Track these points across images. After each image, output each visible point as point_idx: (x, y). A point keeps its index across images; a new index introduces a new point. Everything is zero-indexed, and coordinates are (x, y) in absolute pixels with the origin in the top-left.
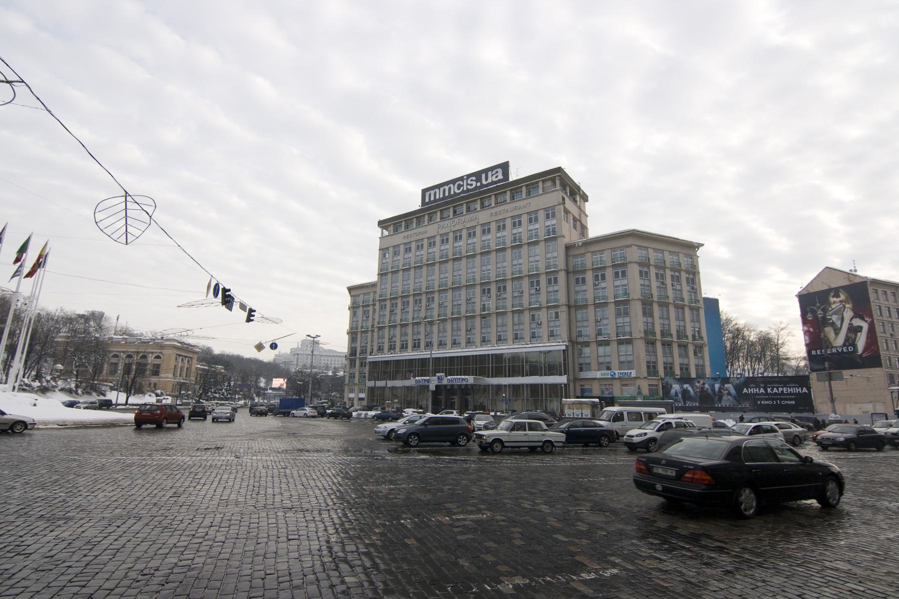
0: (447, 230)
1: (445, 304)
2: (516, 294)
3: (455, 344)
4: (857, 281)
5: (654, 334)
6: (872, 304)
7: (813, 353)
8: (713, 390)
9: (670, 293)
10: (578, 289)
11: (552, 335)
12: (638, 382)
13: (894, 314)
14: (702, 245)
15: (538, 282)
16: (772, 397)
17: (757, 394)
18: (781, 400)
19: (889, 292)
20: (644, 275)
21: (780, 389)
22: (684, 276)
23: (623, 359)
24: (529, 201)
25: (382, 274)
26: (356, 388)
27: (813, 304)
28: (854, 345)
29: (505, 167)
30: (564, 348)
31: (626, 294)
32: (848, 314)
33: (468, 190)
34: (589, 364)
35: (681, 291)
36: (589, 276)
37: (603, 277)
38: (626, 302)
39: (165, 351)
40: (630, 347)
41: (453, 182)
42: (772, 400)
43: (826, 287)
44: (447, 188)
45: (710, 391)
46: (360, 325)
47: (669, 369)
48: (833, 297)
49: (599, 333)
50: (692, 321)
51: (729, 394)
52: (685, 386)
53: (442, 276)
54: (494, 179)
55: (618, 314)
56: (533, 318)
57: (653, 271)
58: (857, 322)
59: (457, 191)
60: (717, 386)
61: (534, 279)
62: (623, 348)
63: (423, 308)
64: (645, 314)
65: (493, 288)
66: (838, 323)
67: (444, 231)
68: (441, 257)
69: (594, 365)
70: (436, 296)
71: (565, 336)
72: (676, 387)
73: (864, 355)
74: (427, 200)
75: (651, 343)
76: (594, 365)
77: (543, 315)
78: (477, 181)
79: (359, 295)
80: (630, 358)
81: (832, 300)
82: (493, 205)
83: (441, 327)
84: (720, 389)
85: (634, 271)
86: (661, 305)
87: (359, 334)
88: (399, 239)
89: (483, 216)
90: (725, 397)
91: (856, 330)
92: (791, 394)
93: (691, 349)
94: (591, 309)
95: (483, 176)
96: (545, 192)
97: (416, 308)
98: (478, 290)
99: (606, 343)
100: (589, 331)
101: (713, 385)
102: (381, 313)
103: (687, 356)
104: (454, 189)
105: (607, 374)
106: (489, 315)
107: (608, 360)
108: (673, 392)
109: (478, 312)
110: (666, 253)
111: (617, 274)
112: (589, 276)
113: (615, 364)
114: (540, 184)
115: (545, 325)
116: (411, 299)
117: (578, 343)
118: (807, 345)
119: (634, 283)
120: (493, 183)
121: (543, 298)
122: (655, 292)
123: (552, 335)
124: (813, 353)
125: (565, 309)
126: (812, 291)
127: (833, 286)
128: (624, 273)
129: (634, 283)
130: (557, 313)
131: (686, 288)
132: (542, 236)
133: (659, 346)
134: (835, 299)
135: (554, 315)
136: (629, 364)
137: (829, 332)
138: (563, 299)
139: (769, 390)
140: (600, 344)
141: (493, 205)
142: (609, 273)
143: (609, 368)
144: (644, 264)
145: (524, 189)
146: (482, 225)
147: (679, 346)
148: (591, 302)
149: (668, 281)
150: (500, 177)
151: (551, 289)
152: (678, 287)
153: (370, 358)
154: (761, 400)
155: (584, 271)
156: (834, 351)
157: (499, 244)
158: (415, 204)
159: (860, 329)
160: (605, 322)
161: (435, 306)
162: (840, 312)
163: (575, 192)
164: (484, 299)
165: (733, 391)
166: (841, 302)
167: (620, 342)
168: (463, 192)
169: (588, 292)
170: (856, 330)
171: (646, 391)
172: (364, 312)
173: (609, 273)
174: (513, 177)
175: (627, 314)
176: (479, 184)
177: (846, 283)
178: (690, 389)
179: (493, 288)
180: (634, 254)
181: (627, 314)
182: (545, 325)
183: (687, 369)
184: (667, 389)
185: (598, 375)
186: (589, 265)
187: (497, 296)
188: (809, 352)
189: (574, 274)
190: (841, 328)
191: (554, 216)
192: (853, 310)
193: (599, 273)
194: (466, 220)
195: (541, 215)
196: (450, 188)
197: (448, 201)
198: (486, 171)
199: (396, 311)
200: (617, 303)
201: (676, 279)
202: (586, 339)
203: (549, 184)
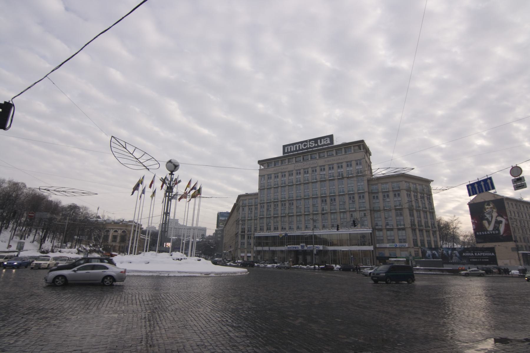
0: (300, 168)
1: (300, 207)
2: (341, 203)
4: (499, 198)
5: (415, 225)
6: (507, 210)
7: (478, 233)
8: (448, 254)
9: (421, 205)
10: (374, 201)
12: (410, 250)
13: (528, 217)
14: (432, 181)
17: (470, 256)
18: (482, 259)
19: (514, 204)
20: (409, 195)
21: (481, 254)
23: (400, 238)
24: (346, 156)
25: (261, 188)
26: (246, 251)
28: (498, 230)
29: (331, 137)
30: (371, 232)
32: (495, 214)
33: (310, 148)
34: (383, 240)
35: (425, 203)
36: (380, 195)
37: (388, 196)
38: (401, 209)
40: (404, 232)
41: (301, 142)
42: (478, 259)
43: (482, 200)
44: (298, 145)
45: (446, 254)
46: (247, 216)
47: (422, 242)
48: (487, 205)
49: (387, 224)
50: (431, 219)
51: (456, 256)
52: (434, 252)
53: (298, 192)
54: (325, 143)
55: (397, 215)
57: (412, 194)
58: (500, 219)
59: (304, 148)
60: (450, 252)
61: (351, 196)
62: (400, 232)
63: (287, 209)
64: (410, 215)
65: (328, 200)
66: (490, 219)
67: (298, 168)
68: (297, 182)
70: (295, 202)
71: (370, 225)
72: (429, 252)
73: (504, 235)
74: (286, 151)
75: (414, 230)
78: (315, 143)
79: (246, 200)
80: (404, 237)
81: (486, 207)
82: (326, 156)
83: (298, 219)
84: (451, 253)
85: (404, 193)
86: (417, 211)
87: (246, 221)
88: (272, 170)
89: (321, 162)
90: (454, 258)
91: (498, 223)
92: (486, 256)
93: (431, 232)
95: (319, 141)
96: (355, 152)
97: (282, 208)
98: (319, 200)
99: (392, 230)
100: (381, 223)
101: (448, 252)
102: (261, 210)
106: (327, 213)
107: (393, 238)
108: (427, 254)
110: (411, 184)
111: (395, 195)
112: (380, 195)
113: (397, 240)
114: (352, 147)
116: (279, 204)
117: (376, 229)
118: (474, 229)
119: (404, 198)
120: (324, 145)
121: (357, 206)
122: (414, 204)
124: (478, 233)
125: (369, 212)
126: (475, 202)
127: (487, 200)
128: (399, 195)
129: (404, 198)
130: (365, 214)
131: (427, 202)
133: (417, 231)
134: (488, 207)
135: (363, 215)
136: (405, 241)
137: (485, 223)
138: (368, 207)
139: (476, 254)
140: (388, 230)
141: (326, 156)
142: (391, 194)
143: (393, 242)
145: (343, 150)
146: (320, 166)
147: (426, 231)
150: (329, 142)
151: (361, 201)
152: (424, 202)
153: (257, 234)
154: (472, 259)
155: (378, 193)
156: (488, 233)
157: (331, 176)
158: (279, 153)
159: (501, 222)
160: (390, 219)
161: (294, 207)
162: (490, 213)
163: (367, 152)
164: (323, 205)
165: (458, 254)
166: (491, 208)
167: (399, 229)
168: (307, 148)
172: (249, 209)
173: (391, 194)
174: (336, 143)
175: (401, 215)
176: (316, 145)
177: (493, 199)
178: (436, 253)
179: (328, 200)
180: (404, 185)
181: (401, 215)
183: (430, 243)
184: (424, 253)
185: (388, 245)
186: (380, 190)
187: (330, 203)
188: (475, 233)
189: (373, 194)
190: (491, 222)
192: (497, 212)
193: (386, 194)
194: (309, 164)
195: (354, 163)
196: (299, 146)
199: (270, 209)
201: (422, 198)
202: (380, 227)
203: (357, 148)
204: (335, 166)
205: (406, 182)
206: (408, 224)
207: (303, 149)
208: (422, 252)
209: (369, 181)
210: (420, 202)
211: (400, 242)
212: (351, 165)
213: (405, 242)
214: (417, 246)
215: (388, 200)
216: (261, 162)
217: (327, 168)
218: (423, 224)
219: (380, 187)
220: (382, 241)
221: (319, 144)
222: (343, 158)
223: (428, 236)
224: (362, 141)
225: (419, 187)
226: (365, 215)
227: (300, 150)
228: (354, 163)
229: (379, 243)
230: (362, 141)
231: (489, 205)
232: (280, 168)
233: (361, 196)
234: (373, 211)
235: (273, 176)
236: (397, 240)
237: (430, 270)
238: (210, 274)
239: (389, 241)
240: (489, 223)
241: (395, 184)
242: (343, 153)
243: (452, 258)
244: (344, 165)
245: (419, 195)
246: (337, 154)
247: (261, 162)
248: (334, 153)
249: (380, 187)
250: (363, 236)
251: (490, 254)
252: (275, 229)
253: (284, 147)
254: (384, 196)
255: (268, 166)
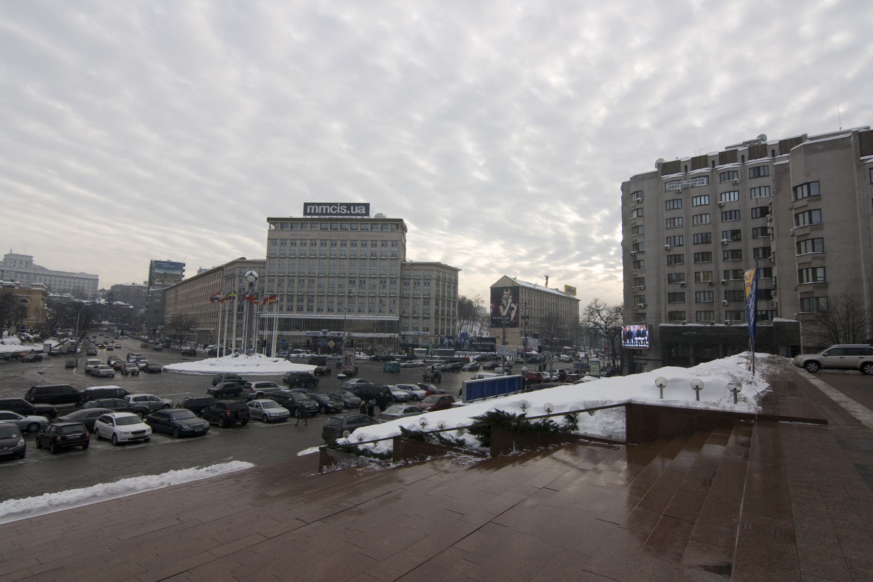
11: (391, 311)
15: (385, 282)
25: (269, 257)
27: (497, 292)
29: (367, 206)
32: (510, 301)
36: (412, 282)
39: (33, 296)
41: (330, 205)
49: (414, 312)
55: (424, 304)
62: (425, 321)
63: (306, 285)
69: (410, 328)
72: (446, 340)
75: (437, 319)
76: (410, 328)
77: (387, 301)
89: (353, 235)
99: (418, 318)
100: (409, 311)
104: (330, 210)
109: (346, 294)
112: (412, 282)
113: (421, 328)
116: (296, 279)
123: (391, 311)
137: (501, 307)
140: (414, 318)
142: (422, 282)
144: (438, 279)
162: (507, 299)
170: (513, 309)
175: (428, 304)
182: (387, 306)
184: (442, 341)
185: (412, 333)
186: (412, 277)
191: (396, 245)
195: (389, 244)
200: (424, 298)
203: (394, 226)
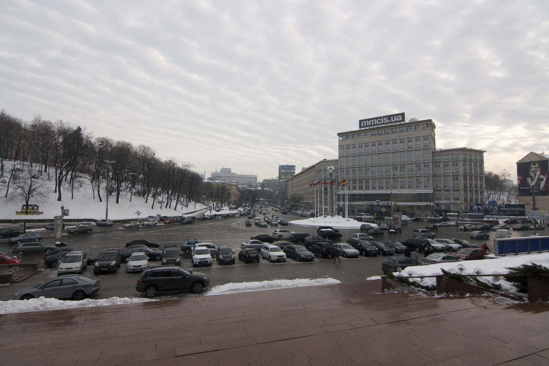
0: (375, 141)
3: (380, 188)
5: (467, 187)
9: (473, 171)
10: (436, 169)
11: (426, 187)
12: (460, 205)
16: (512, 211)
20: (465, 165)
22: (478, 164)
23: (455, 196)
28: (539, 187)
29: (403, 115)
31: (457, 172)
32: (538, 173)
36: (442, 165)
37: (448, 165)
40: (458, 192)
41: (376, 118)
43: (530, 161)
44: (373, 121)
49: (445, 186)
55: (454, 180)
56: (417, 180)
58: (542, 177)
60: (491, 207)
62: (455, 193)
65: (399, 168)
66: (533, 177)
70: (370, 169)
71: (432, 187)
72: (475, 207)
74: (362, 125)
75: (466, 191)
76: (443, 198)
78: (388, 120)
80: (458, 196)
81: (532, 166)
85: (461, 164)
88: (349, 142)
89: (393, 136)
91: (540, 180)
93: (479, 192)
94: (442, 177)
95: (392, 118)
98: (391, 168)
100: (441, 185)
103: (478, 195)
104: (377, 122)
105: (448, 202)
107: (449, 196)
111: (454, 165)
112: (442, 165)
113: (452, 198)
115: (423, 183)
120: (397, 122)
122: (468, 171)
124: (521, 188)
126: (523, 162)
127: (533, 160)
128: (457, 165)
132: (422, 147)
133: (468, 192)
137: (529, 180)
143: (449, 200)
148: (442, 174)
149: (473, 167)
155: (440, 162)
162: (535, 172)
165: (497, 209)
168: (381, 124)
169: (441, 171)
171: (463, 208)
174: (407, 120)
175: (457, 179)
177: (539, 160)
179: (399, 168)
180: (461, 157)
182: (423, 183)
184: (471, 207)
185: (444, 202)
186: (442, 160)
189: (436, 164)
192: (541, 171)
193: (446, 164)
195: (422, 138)
196: (374, 122)
197: (373, 128)
198: (393, 116)
201: (475, 165)
202: (439, 189)
203: (425, 125)
204: (406, 140)
205: (464, 154)
206: (461, 186)
207: (377, 124)
208: (470, 207)
209: (433, 153)
210: (473, 169)
211: (455, 200)
212: (419, 140)
213: (458, 200)
214: (467, 202)
215: (448, 168)
216: (339, 134)
217: (398, 141)
218: (474, 186)
219: (442, 158)
220: (440, 199)
221: (392, 121)
222: (412, 133)
223: (477, 194)
224: (430, 120)
225: (473, 157)
226: (428, 179)
227: (374, 125)
228: (422, 138)
229: (437, 200)
230: (430, 120)
231: (534, 165)
232: (357, 140)
233: (426, 165)
234: (434, 176)
235: (351, 147)
236: (452, 198)
237: (474, 221)
238: (444, 258)
239: (446, 199)
240: (532, 180)
241: (454, 156)
242: (413, 130)
243: (492, 212)
244: (414, 139)
245: (473, 164)
246: (407, 130)
247: (339, 134)
248: (405, 129)
249: (442, 158)
250: (427, 195)
251: (521, 209)
252: (353, 188)
253: (361, 121)
254: (445, 165)
255: (347, 138)
